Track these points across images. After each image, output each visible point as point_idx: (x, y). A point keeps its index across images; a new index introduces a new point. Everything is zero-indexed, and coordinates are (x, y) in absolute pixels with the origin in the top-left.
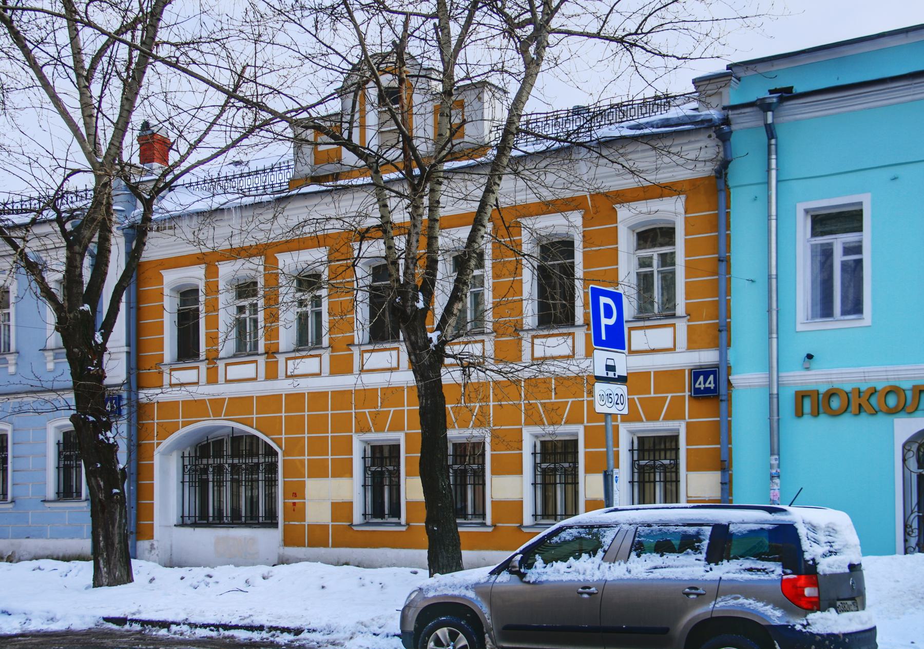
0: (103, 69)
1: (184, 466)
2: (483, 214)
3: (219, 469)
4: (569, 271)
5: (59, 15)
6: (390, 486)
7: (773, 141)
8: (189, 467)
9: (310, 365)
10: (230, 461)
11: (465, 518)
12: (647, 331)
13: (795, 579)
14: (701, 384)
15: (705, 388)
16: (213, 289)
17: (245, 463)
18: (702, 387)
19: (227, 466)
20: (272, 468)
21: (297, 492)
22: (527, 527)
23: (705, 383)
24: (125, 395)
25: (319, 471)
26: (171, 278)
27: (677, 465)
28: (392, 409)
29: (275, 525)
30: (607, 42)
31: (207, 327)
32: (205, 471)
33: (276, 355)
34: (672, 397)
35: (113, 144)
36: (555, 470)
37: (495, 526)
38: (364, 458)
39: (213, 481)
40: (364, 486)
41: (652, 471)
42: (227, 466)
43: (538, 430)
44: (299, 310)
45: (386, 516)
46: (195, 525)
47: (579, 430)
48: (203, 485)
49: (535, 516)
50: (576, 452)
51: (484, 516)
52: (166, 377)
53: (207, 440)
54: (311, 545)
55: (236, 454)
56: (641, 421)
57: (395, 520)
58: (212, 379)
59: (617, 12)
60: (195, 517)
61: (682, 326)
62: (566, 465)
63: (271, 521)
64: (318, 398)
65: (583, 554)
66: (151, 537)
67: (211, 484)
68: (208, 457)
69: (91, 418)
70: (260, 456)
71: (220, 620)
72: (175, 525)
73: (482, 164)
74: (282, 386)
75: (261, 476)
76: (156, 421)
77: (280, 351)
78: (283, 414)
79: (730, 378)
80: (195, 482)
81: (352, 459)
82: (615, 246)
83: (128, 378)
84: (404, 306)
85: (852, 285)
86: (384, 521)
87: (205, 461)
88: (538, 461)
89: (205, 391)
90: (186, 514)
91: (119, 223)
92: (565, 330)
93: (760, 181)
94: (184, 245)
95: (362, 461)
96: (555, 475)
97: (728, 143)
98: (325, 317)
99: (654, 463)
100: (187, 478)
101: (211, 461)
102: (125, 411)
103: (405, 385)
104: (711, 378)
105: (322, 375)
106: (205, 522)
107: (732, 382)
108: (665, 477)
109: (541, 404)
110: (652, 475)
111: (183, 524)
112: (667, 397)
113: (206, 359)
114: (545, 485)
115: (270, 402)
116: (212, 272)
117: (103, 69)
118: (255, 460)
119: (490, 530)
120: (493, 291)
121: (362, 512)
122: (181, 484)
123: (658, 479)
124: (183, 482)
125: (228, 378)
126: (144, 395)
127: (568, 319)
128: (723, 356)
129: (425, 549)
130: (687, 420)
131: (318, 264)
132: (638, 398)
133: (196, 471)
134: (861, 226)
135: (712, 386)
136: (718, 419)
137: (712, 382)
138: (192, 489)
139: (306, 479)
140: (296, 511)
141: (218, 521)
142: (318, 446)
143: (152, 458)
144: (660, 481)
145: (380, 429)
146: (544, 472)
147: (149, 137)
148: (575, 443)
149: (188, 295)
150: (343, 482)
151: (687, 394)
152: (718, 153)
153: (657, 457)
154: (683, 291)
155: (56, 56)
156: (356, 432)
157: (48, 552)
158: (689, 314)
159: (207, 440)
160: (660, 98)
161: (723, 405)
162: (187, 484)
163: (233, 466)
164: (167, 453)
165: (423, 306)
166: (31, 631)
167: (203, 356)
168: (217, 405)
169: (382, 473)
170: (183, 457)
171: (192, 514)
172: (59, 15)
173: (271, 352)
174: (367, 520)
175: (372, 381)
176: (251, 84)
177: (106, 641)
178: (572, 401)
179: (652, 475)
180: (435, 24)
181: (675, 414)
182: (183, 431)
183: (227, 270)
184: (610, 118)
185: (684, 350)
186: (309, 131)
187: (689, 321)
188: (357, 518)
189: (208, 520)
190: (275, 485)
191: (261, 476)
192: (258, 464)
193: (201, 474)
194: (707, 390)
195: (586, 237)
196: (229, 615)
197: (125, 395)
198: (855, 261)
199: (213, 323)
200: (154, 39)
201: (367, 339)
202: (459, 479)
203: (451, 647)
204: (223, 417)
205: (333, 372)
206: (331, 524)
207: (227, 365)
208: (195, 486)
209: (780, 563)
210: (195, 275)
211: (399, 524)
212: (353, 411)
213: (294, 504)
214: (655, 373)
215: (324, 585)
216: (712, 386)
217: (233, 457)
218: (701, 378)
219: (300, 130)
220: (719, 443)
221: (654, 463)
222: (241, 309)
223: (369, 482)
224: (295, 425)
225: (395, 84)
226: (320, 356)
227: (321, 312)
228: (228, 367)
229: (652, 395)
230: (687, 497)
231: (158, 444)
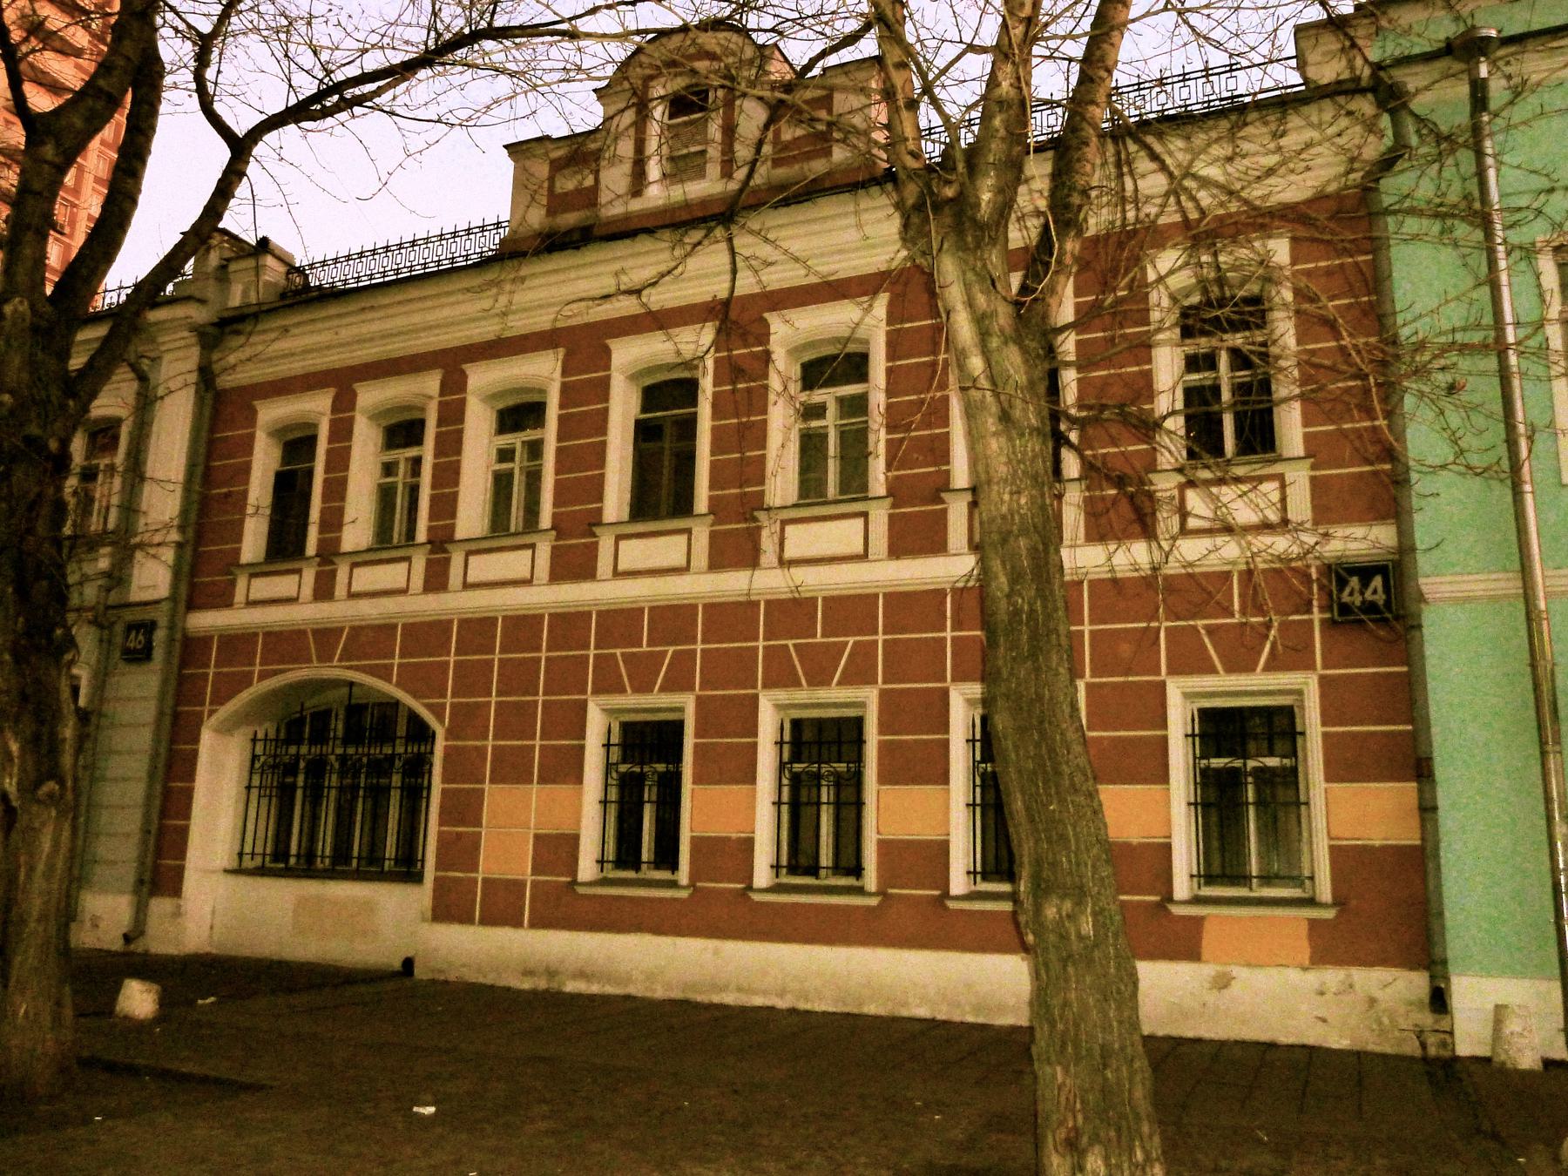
0: (177, 30)
1: (254, 758)
2: (1105, 46)
3: (317, 768)
4: (688, 427)
5: (754, 30)
6: (838, 805)
8: (262, 759)
9: (513, 564)
10: (339, 751)
11: (637, 869)
13: (893, 887)
14: (1352, 594)
15: (1363, 602)
16: (453, 414)
17: (369, 755)
18: (1358, 600)
19: (333, 758)
20: (418, 767)
21: (464, 809)
22: (957, 898)
24: (163, 621)
25: (512, 769)
26: (271, 413)
29: (416, 878)
30: (1517, 566)
31: (326, 497)
32: (292, 769)
34: (855, 643)
35: (341, 854)
36: (818, 776)
38: (607, 746)
39: (305, 788)
41: (815, 782)
42: (333, 758)
43: (782, 695)
44: (1313, 473)
45: (644, 867)
46: (261, 872)
47: (687, 704)
48: (285, 796)
49: (776, 867)
50: (860, 742)
51: (857, 871)
52: (768, 543)
53: (302, 710)
54: (489, 920)
55: (353, 735)
56: (1213, 671)
58: (436, 580)
60: (264, 855)
61: (880, 515)
62: (841, 767)
63: (408, 870)
64: (523, 627)
66: (176, 892)
67: (299, 793)
68: (299, 743)
70: (398, 741)
72: (226, 871)
74: (455, 603)
75: (396, 780)
76: (541, 698)
77: (1409, 836)
78: (948, 634)
81: (947, 741)
82: (1163, 733)
85: (1003, 604)
86: (641, 875)
87: (293, 750)
88: (614, 758)
89: (309, 613)
90: (248, 849)
92: (289, 566)
94: (787, 267)
95: (602, 751)
96: (819, 787)
97: (271, 247)
98: (879, 440)
100: (256, 781)
101: (304, 750)
102: (158, 654)
103: (948, 587)
104: (1377, 582)
105: (535, 582)
106: (282, 865)
108: (837, 795)
109: (1211, 630)
110: (814, 791)
111: (238, 871)
112: (847, 643)
113: (317, 556)
114: (795, 806)
115: (427, 635)
116: (454, 384)
117: (177, 30)
118: (388, 750)
119: (874, 902)
120: (794, 600)
121: (596, 854)
122: (244, 791)
123: (824, 799)
124: (249, 788)
125: (470, 579)
126: (205, 621)
127: (682, 505)
128: (1405, 533)
129: (122, 892)
132: (795, 645)
133: (274, 767)
135: (1380, 598)
137: (1380, 589)
138: (264, 801)
139: (487, 786)
140: (460, 852)
141: (307, 869)
142: (515, 720)
143: (196, 739)
144: (329, 787)
145: (643, 687)
146: (796, 780)
147: (1243, 375)
148: (678, 726)
149: (298, 445)
150: (563, 790)
151: (1317, 616)
152: (1422, 394)
153: (825, 756)
155: (1512, 123)
156: (953, 680)
157: (352, 305)
158: (715, 507)
159: (302, 710)
162: (254, 792)
163: (343, 759)
164: (226, 729)
166: (145, 463)
168: (326, 636)
169: (641, 778)
170: (254, 740)
171: (259, 850)
172: (754, 30)
173: (441, 541)
174: (604, 874)
175: (370, 611)
176: (1176, 529)
177: (1019, 796)
179: (814, 791)
180: (1369, 37)
181: (1293, 656)
182: (258, 688)
183: (370, 396)
184: (483, 239)
188: (587, 869)
189: (287, 862)
190: (1298, 804)
191: (396, 780)
192: (391, 759)
193: (285, 775)
194: (1370, 608)
195: (565, 388)
197: (163, 621)
199: (336, 490)
200: (1217, 237)
201: (626, 517)
202: (786, 790)
204: (335, 663)
205: (897, 550)
206: (529, 879)
207: (619, 538)
208: (270, 796)
209: (155, 987)
210: (317, 406)
212: (880, 638)
213: (459, 835)
216: (1380, 598)
217: (346, 742)
222: (389, 469)
223: (613, 794)
224: (474, 678)
226: (532, 546)
227: (476, 847)
228: (472, 559)
229: (819, 639)
230: (1331, 838)
231: (211, 713)
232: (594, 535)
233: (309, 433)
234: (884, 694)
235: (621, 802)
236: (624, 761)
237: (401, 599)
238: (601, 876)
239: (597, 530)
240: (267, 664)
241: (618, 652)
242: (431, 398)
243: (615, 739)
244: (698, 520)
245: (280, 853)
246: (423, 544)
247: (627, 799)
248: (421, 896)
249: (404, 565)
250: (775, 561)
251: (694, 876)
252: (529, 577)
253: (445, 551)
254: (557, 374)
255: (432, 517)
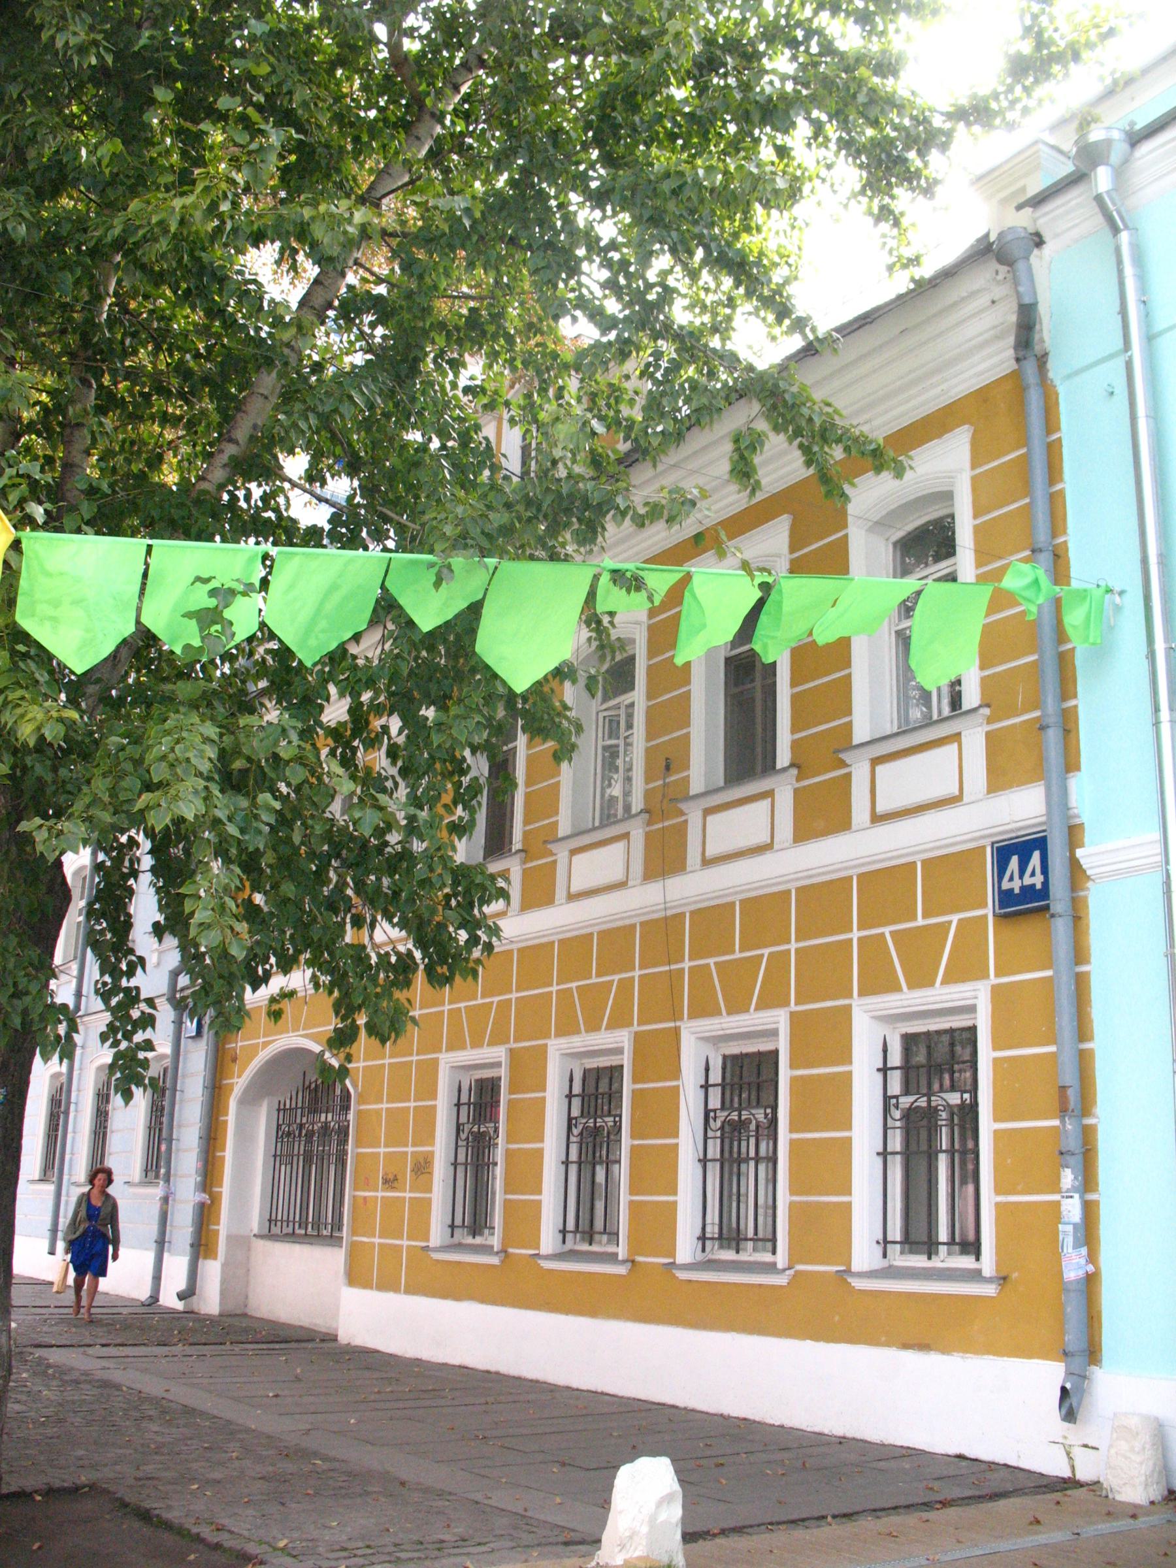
7: (1124, 236)
8: (722, 1115)
12: (1066, 1473)
15: (1022, 888)
18: (1016, 885)
22: (860, 1275)
23: (1021, 877)
27: (774, 1122)
28: (955, 918)
33: (683, 806)
37: (633, 1261)
40: (884, 1154)
57: (966, 1262)
59: (907, 608)
65: (520, 685)
69: (192, 1557)
71: (1115, 1487)
73: (1088, 1150)
79: (1079, 853)
80: (469, 1104)
83: (1049, 813)
84: (717, 73)
86: (936, 1263)
91: (472, 298)
93: (1168, 335)
99: (929, 1101)
104: (1036, 855)
107: (1085, 863)
113: (792, 765)
122: (563, 1167)
127: (769, 766)
128: (1058, 800)
130: (793, 1007)
131: (359, 1552)
134: (366, 1285)
135: (1038, 880)
136: (1049, 973)
137: (1038, 870)
144: (469, 1104)
145: (921, 978)
153: (936, 1086)
154: (558, 891)
160: (617, 402)
161: (1061, 928)
165: (317, 270)
167: (783, 757)
169: (931, 1113)
174: (456, 1239)
178: (770, 954)
185: (981, 796)
186: (304, 522)
187: (990, 720)
196: (677, 35)
198: (365, 1103)
203: (667, 4)
205: (803, 833)
211: (975, 1275)
212: (377, 1240)
214: (926, 863)
215: (1115, 397)
216: (1038, 880)
218: (1014, 861)
219: (250, 110)
220: (1053, 1041)
221: (929, 1101)
223: (896, 1142)
225: (800, 38)
228: (880, 769)
232: (844, 764)
233: (934, 513)
234: (996, 990)
235: (908, 1155)
236: (907, 1092)
237: (768, 857)
238: (884, 1263)
239: (846, 757)
240: (646, 967)
241: (887, 930)
242: (779, 556)
243: (716, 1077)
244: (781, 777)
245: (303, 1224)
246: (784, 770)
247: (913, 1147)
248: (331, 1260)
249: (765, 804)
250: (866, 816)
251: (636, 1245)
252: (957, 793)
253: (843, 764)
254: (967, 464)
255: (526, 822)
